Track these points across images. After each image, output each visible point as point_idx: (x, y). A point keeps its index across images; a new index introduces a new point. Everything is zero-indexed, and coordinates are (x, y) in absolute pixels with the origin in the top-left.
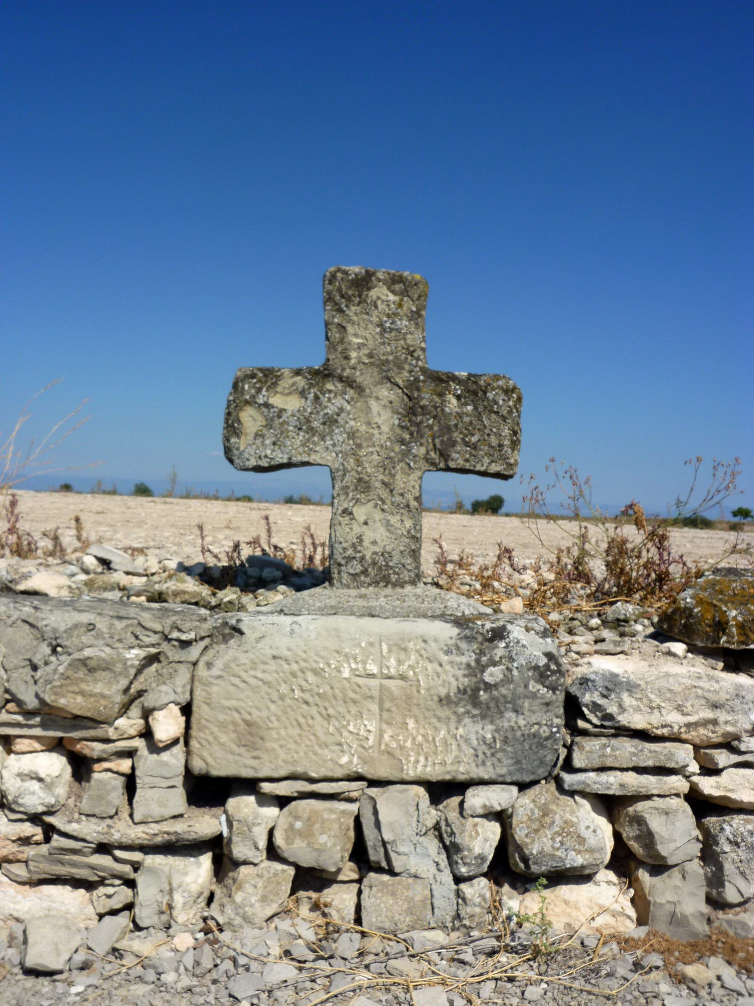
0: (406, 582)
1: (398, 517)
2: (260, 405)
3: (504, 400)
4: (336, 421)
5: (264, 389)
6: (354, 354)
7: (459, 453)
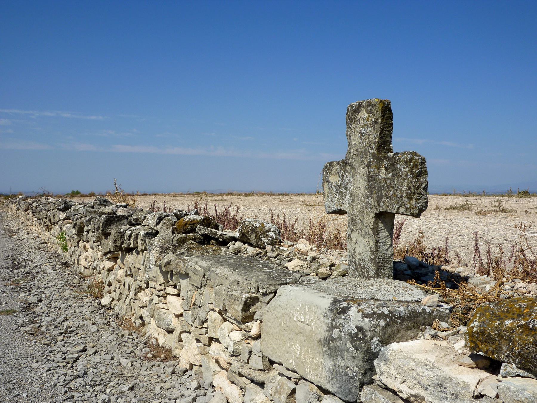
0: (371, 277)
1: (367, 240)
3: (404, 168)
7: (383, 202)
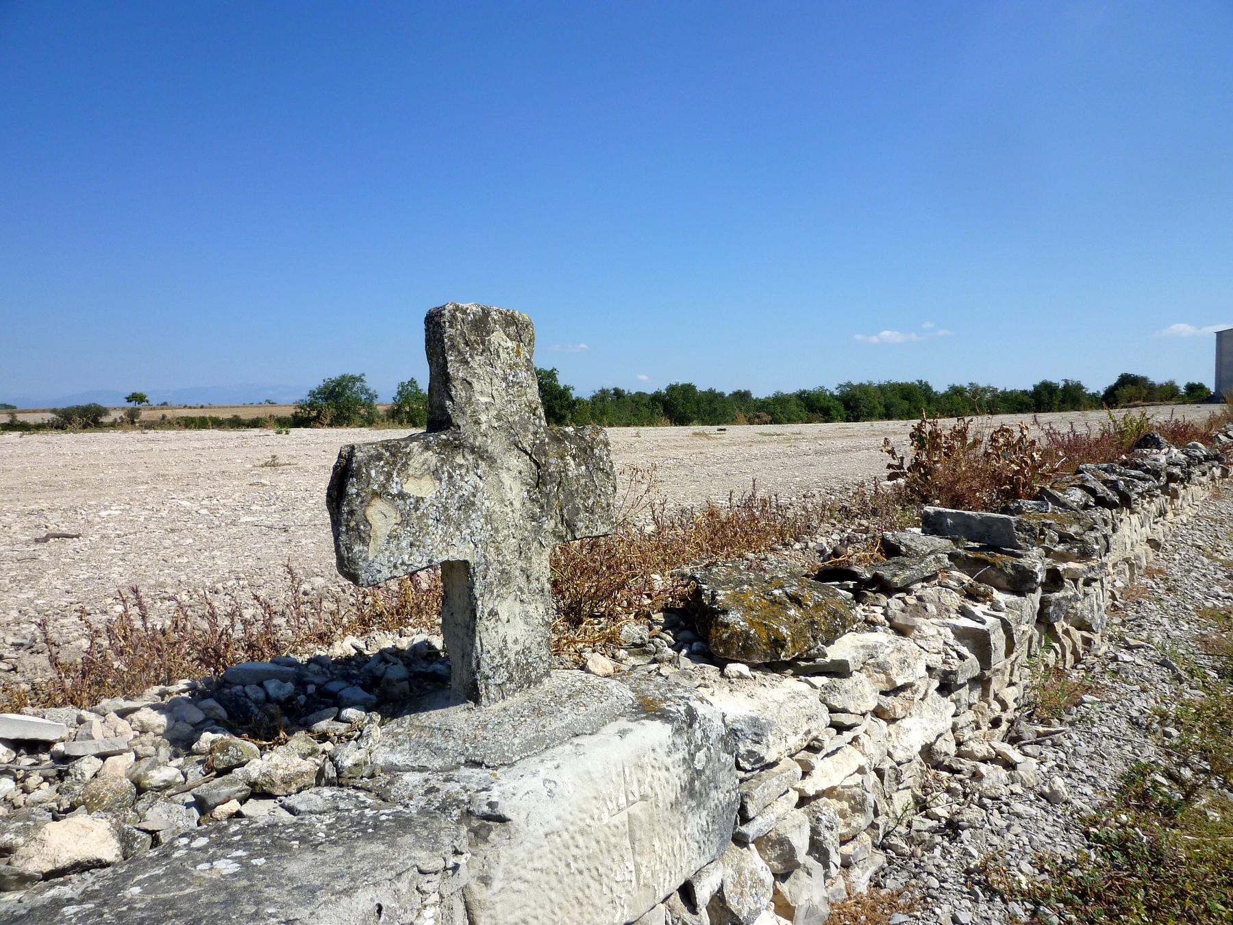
2: (394, 496)
4: (473, 504)
5: (395, 474)
6: (483, 418)
